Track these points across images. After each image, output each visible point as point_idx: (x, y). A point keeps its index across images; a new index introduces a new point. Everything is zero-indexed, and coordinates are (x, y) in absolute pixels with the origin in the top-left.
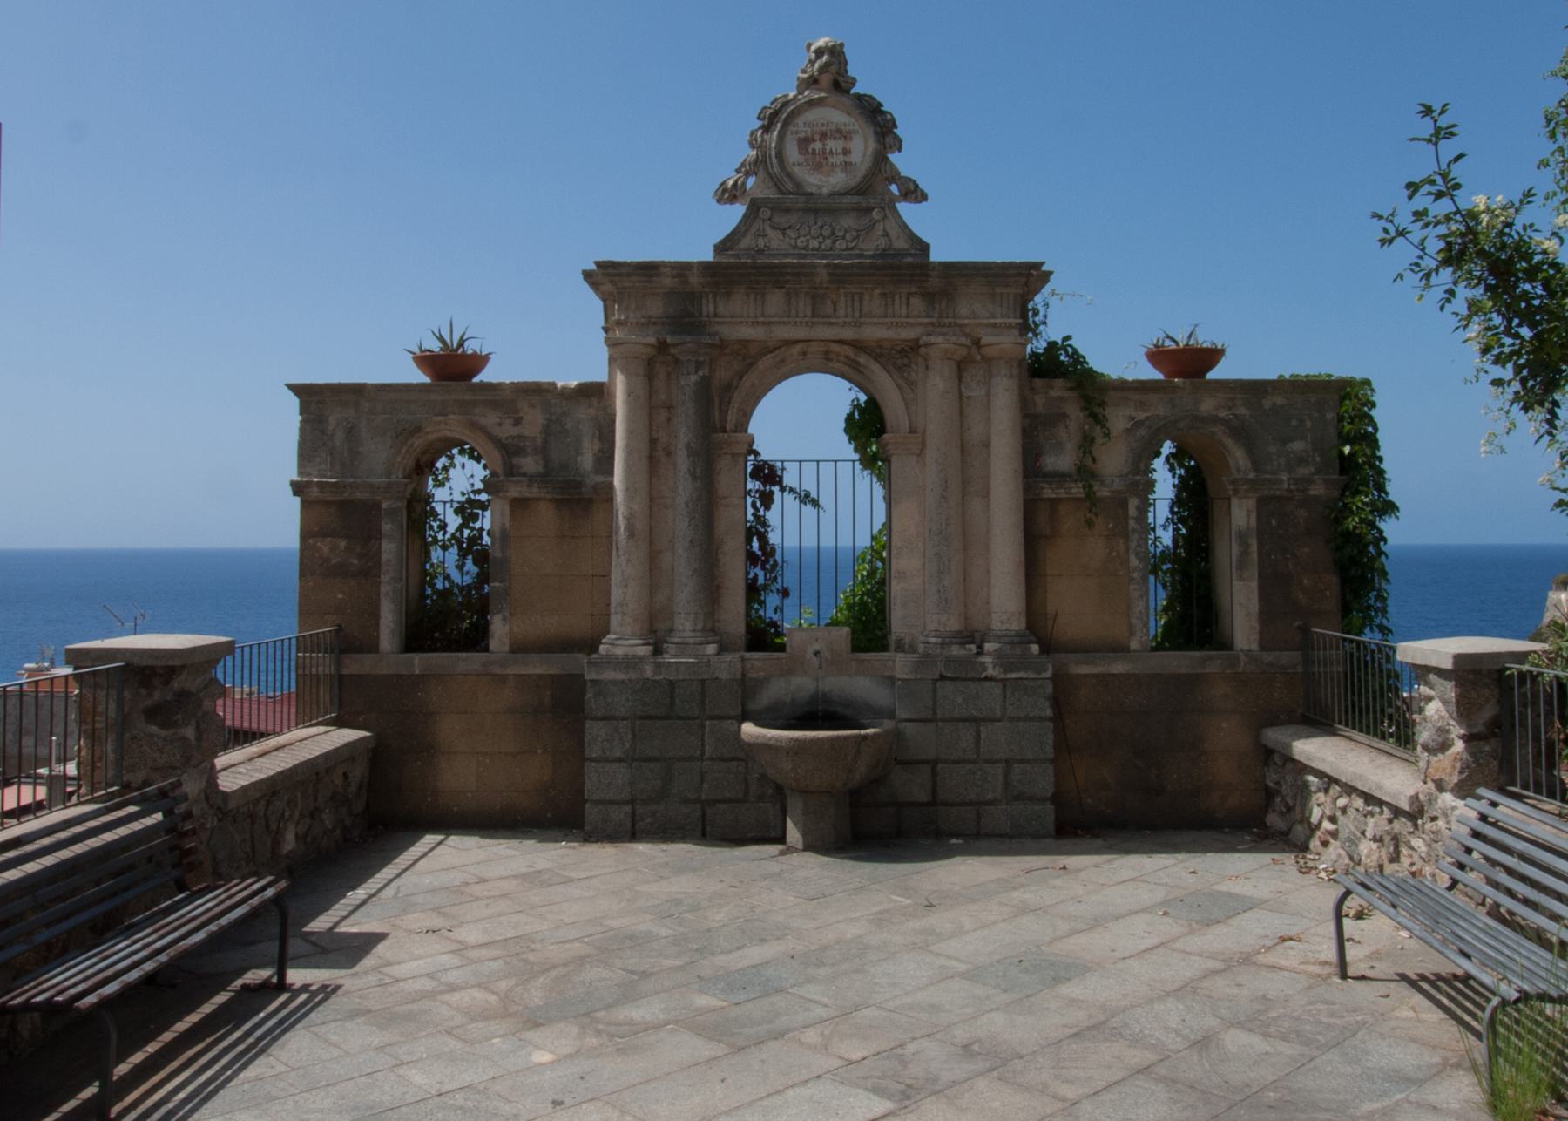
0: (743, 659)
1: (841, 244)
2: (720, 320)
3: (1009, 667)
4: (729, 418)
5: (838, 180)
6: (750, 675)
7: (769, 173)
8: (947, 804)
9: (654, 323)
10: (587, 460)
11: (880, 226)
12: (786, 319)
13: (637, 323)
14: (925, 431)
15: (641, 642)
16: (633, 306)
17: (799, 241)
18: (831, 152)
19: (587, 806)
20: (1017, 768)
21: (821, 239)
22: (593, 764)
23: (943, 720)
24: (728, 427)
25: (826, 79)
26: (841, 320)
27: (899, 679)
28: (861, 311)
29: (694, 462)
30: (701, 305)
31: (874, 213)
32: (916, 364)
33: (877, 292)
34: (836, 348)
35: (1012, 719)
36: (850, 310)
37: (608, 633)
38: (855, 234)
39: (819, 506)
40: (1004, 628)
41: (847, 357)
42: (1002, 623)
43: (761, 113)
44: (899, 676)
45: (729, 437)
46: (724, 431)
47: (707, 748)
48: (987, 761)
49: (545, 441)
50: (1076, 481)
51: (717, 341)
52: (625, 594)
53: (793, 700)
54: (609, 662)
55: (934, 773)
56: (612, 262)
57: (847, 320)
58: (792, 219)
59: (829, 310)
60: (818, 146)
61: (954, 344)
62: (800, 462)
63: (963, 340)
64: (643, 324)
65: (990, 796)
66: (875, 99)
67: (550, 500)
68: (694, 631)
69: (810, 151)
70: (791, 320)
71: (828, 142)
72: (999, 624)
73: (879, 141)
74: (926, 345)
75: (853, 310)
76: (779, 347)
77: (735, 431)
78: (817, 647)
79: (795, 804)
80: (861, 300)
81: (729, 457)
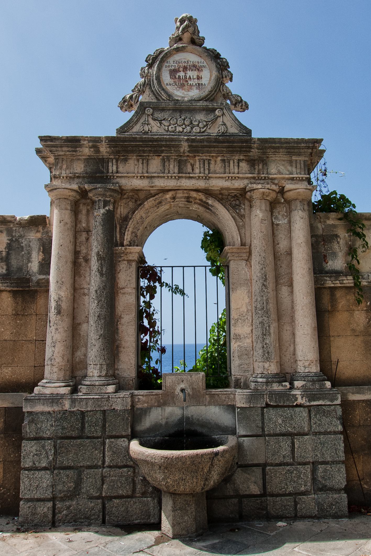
0: (132, 396)
1: (196, 130)
2: (120, 175)
3: (312, 397)
4: (126, 237)
5: (194, 93)
6: (137, 406)
7: (152, 91)
8: (272, 495)
9: (78, 177)
10: (34, 266)
11: (220, 120)
12: (162, 175)
13: (67, 177)
14: (251, 245)
15: (63, 384)
16: (64, 167)
17: (170, 128)
18: (190, 78)
19: (21, 503)
20: (321, 468)
21: (184, 126)
22: (26, 472)
23: (269, 435)
24: (125, 243)
25: (187, 36)
26: (196, 175)
27: (238, 408)
28: (209, 170)
29: (101, 264)
30: (108, 166)
31: (217, 111)
32: (244, 205)
33: (219, 158)
34: (194, 194)
35: (316, 434)
36: (202, 169)
37: (43, 378)
38: (205, 123)
39: (185, 294)
40: (306, 371)
41: (201, 200)
42: (305, 367)
43: (147, 58)
44: (238, 405)
45: (126, 249)
46: (122, 245)
47: (107, 459)
48: (300, 464)
49: (8, 254)
50: (346, 276)
51: (117, 188)
52: (54, 352)
53: (167, 423)
54: (39, 399)
55: (264, 474)
56: (50, 137)
57: (201, 175)
58: (166, 115)
59: (189, 169)
60: (182, 74)
61: (268, 189)
62: (172, 267)
63: (274, 187)
64: (70, 177)
65: (303, 489)
66: (216, 51)
67: (10, 291)
68: (100, 376)
69: (177, 77)
70: (165, 175)
71: (188, 72)
72: (303, 368)
73: (219, 72)
74: (250, 191)
75: (204, 170)
76: (157, 194)
77: (130, 245)
78: (182, 386)
79: (167, 503)
80: (209, 164)
81: (125, 262)
